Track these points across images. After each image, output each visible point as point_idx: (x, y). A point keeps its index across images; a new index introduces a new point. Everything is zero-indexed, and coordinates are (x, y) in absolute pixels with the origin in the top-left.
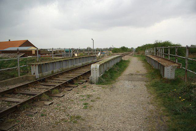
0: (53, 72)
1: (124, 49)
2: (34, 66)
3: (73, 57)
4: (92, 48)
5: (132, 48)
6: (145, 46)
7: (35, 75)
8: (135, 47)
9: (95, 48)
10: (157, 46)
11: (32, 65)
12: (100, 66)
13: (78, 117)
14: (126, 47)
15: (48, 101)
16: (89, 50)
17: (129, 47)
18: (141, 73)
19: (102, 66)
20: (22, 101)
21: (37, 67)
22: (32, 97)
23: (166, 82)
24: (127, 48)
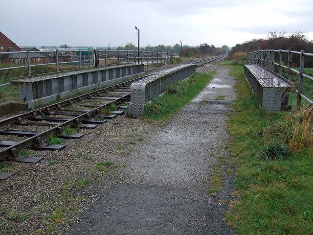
0: (58, 97)
1: (205, 50)
2: (24, 85)
3: (96, 67)
4: (137, 46)
5: (225, 47)
6: (251, 43)
7: (26, 103)
8: (231, 44)
9: (143, 45)
10: (276, 43)
11: (20, 82)
12: (146, 87)
13: (108, 165)
14: (210, 44)
15: (59, 143)
16: (130, 47)
17: (218, 45)
18: (227, 99)
19: (151, 86)
20: (13, 144)
21: (30, 88)
22: (7, 149)
23: (67, 166)
24: (213, 46)
